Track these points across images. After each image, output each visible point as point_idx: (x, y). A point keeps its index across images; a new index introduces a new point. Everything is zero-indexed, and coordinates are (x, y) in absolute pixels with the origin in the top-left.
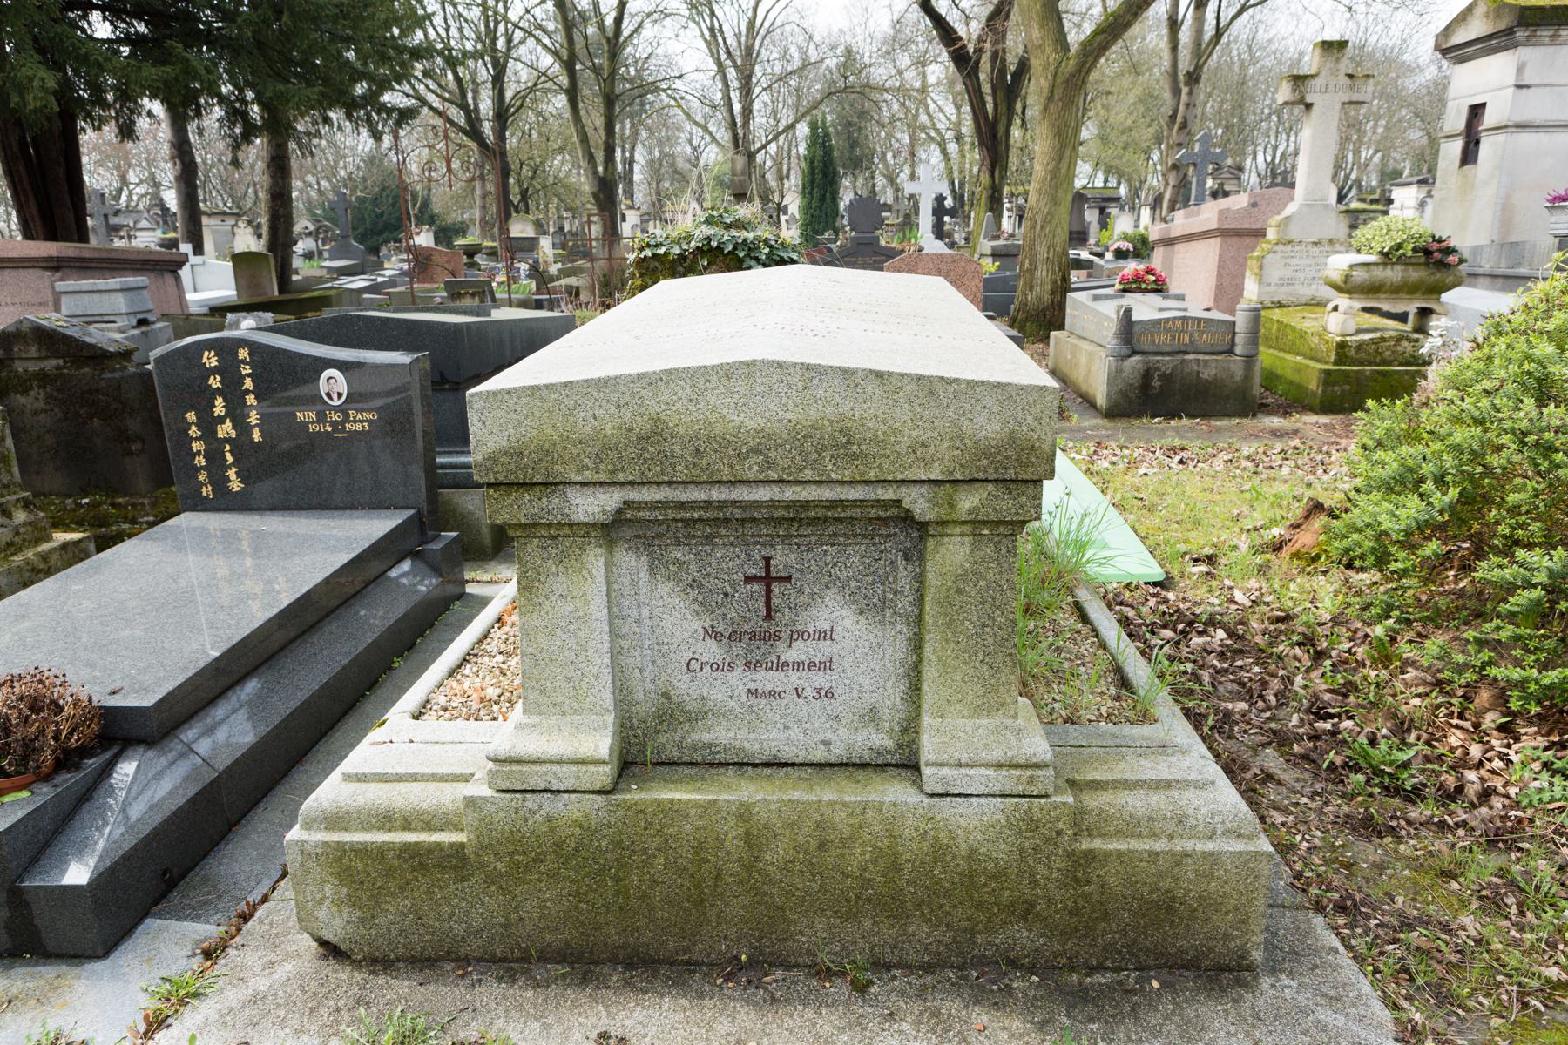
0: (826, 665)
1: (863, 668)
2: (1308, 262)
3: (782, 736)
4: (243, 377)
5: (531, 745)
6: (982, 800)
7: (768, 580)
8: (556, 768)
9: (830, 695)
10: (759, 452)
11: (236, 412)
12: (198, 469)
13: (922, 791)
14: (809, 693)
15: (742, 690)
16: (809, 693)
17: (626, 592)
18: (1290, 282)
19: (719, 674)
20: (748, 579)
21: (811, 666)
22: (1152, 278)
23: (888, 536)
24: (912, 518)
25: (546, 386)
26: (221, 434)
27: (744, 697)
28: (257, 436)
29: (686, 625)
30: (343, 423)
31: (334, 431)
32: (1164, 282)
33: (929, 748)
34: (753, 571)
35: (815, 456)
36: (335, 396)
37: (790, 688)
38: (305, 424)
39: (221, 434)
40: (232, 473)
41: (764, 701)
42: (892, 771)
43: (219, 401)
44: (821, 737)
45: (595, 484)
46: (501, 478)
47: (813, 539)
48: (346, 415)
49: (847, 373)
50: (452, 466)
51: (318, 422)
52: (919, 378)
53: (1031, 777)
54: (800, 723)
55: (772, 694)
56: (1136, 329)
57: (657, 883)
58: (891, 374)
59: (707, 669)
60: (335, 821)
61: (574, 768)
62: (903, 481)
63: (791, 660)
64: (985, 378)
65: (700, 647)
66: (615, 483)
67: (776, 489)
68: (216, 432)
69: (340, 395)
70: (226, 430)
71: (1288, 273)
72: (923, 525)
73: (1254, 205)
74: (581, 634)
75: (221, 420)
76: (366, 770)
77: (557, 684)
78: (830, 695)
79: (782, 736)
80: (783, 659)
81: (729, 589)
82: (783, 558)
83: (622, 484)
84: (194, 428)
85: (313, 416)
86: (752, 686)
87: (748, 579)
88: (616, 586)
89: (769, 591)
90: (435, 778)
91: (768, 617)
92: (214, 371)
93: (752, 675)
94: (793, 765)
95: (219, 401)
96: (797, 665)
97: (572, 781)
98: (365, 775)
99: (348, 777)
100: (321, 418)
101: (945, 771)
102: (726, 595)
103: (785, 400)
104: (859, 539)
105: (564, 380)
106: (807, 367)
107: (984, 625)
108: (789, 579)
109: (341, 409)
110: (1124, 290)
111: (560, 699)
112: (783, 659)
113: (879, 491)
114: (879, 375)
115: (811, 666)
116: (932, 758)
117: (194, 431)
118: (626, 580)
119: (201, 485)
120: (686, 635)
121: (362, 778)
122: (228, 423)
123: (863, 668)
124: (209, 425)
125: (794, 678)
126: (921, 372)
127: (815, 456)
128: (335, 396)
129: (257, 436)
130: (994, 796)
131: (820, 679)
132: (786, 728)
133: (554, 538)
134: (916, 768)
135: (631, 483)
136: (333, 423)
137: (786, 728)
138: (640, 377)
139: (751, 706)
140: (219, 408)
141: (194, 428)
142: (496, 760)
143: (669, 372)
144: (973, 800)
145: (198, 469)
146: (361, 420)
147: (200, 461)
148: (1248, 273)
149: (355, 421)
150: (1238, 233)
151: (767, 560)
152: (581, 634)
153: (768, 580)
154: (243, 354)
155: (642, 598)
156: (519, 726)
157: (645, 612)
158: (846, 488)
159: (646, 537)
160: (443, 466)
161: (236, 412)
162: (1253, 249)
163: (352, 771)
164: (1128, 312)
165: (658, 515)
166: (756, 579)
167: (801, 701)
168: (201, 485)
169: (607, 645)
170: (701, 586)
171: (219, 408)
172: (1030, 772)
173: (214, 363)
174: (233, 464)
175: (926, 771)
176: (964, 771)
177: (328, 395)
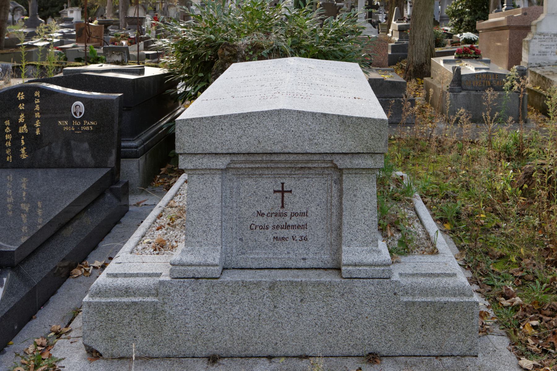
0: (304, 227)
1: (319, 228)
2: (553, 43)
3: (287, 256)
4: (36, 105)
5: (188, 258)
6: (365, 280)
7: (283, 192)
8: (197, 268)
9: (306, 239)
10: (282, 142)
11: (30, 121)
12: (6, 148)
13: (342, 277)
14: (298, 238)
15: (271, 237)
16: (298, 238)
17: (228, 196)
18: (544, 53)
19: (263, 230)
20: (275, 192)
21: (299, 227)
22: (473, 51)
23: (328, 174)
24: (337, 167)
25: (205, 118)
26: (21, 131)
27: (272, 240)
28: (38, 132)
29: (250, 210)
30: (80, 126)
31: (75, 130)
32: (479, 54)
33: (346, 258)
34: (277, 189)
35: (302, 144)
36: (78, 114)
37: (290, 236)
38: (62, 127)
39: (21, 131)
40: (23, 150)
41: (280, 242)
42: (331, 271)
43: (22, 116)
44: (302, 257)
45: (220, 154)
46: (186, 151)
47: (300, 175)
48: (82, 123)
49: (313, 114)
50: (130, 147)
51: (68, 126)
52: (339, 116)
53: (383, 270)
54: (294, 251)
55: (283, 238)
56: (463, 79)
57: (235, 318)
58: (329, 114)
59: (258, 228)
60: (99, 293)
61: (205, 268)
62: (333, 153)
63: (291, 224)
64: (362, 116)
65: (255, 219)
66: (228, 154)
67: (287, 156)
68: (18, 130)
69: (80, 113)
70: (23, 129)
71: (543, 49)
72: (341, 170)
73: (525, 14)
74: (210, 213)
75: (22, 125)
76: (116, 272)
77: (199, 234)
78: (306, 239)
79: (287, 256)
80: (288, 224)
81: (268, 196)
82: (289, 183)
83: (230, 154)
84: (8, 128)
85: (66, 123)
86: (275, 235)
87: (275, 192)
88: (224, 194)
89: (283, 196)
90: (146, 275)
91: (283, 207)
92: (22, 101)
93: (275, 231)
94: (291, 268)
95: (22, 116)
96: (293, 227)
97: (204, 273)
98: (117, 274)
99: (109, 275)
100: (70, 124)
101: (350, 268)
102: (266, 198)
103: (291, 123)
104: (317, 176)
105: (211, 115)
106: (299, 112)
107: (365, 209)
108: (291, 191)
109: (81, 120)
110: (460, 58)
111: (200, 240)
112: (288, 224)
113: (325, 157)
114: (325, 115)
115: (299, 227)
116: (345, 262)
117: (8, 130)
118: (228, 191)
119: (7, 155)
120: (250, 214)
121: (116, 276)
122: (25, 126)
123: (319, 228)
124: (15, 125)
125: (292, 232)
126: (339, 114)
127: (302, 144)
128: (78, 114)
129: (38, 132)
130: (369, 278)
131: (302, 233)
132: (288, 253)
133: (203, 174)
134: (339, 269)
135: (234, 154)
136: (76, 127)
137: (288, 253)
138: (239, 114)
139: (274, 244)
140: (21, 119)
141: (8, 128)
142: (173, 265)
143: (250, 113)
144: (361, 280)
145: (6, 148)
146: (89, 125)
147: (9, 144)
148: (523, 49)
149: (86, 126)
150: (518, 28)
151: (283, 184)
152: (210, 213)
153: (283, 192)
154: (37, 94)
155: (234, 199)
156: (183, 251)
157: (235, 205)
158: (313, 156)
159: (237, 174)
160: (124, 147)
161: (30, 121)
162: (525, 36)
163: (110, 272)
164: (459, 70)
165: (243, 166)
166: (278, 191)
167: (294, 242)
168: (7, 155)
169: (220, 217)
170: (257, 194)
171: (21, 119)
172: (383, 268)
173: (22, 98)
174: (24, 146)
175: (343, 268)
176: (357, 268)
177: (75, 113)
